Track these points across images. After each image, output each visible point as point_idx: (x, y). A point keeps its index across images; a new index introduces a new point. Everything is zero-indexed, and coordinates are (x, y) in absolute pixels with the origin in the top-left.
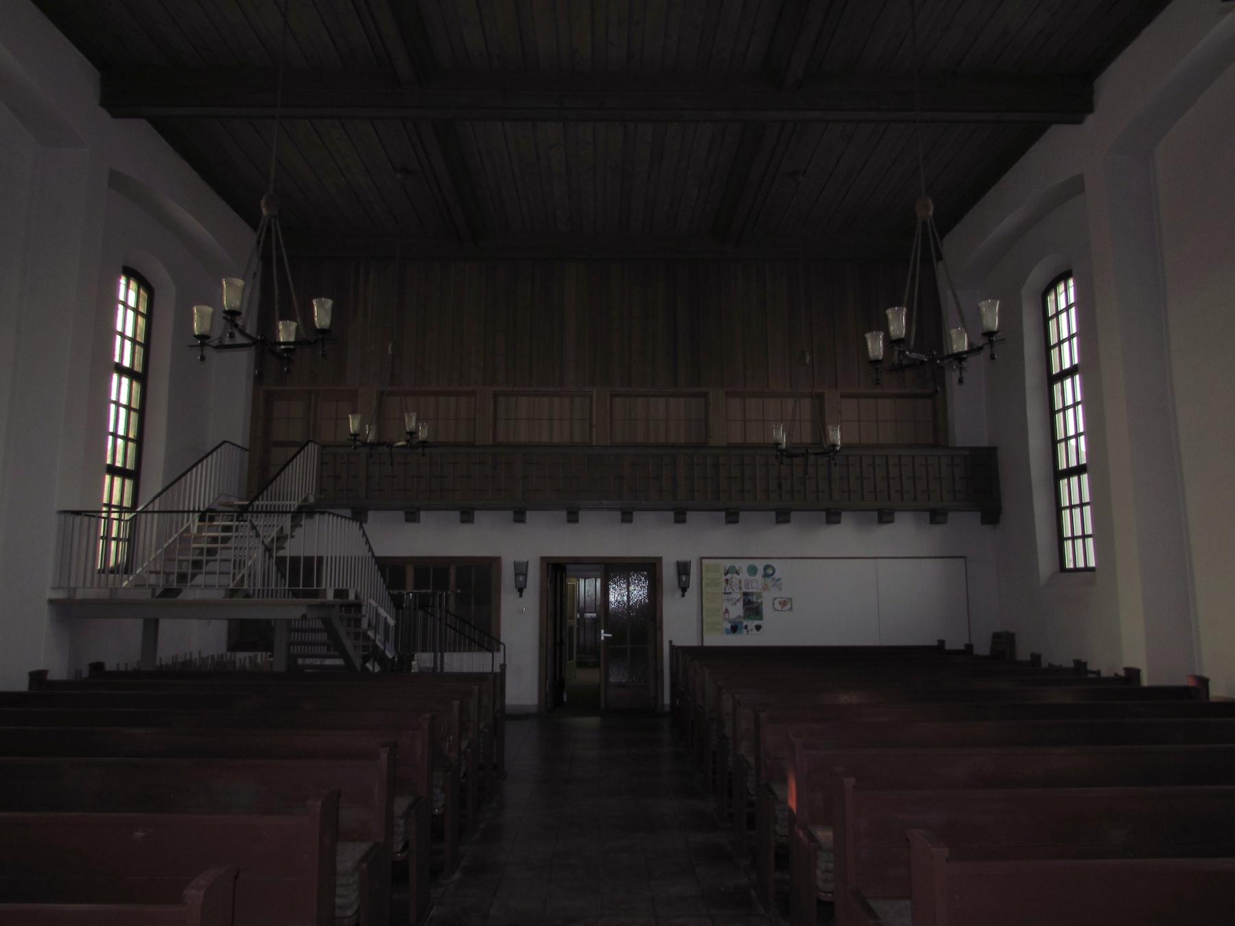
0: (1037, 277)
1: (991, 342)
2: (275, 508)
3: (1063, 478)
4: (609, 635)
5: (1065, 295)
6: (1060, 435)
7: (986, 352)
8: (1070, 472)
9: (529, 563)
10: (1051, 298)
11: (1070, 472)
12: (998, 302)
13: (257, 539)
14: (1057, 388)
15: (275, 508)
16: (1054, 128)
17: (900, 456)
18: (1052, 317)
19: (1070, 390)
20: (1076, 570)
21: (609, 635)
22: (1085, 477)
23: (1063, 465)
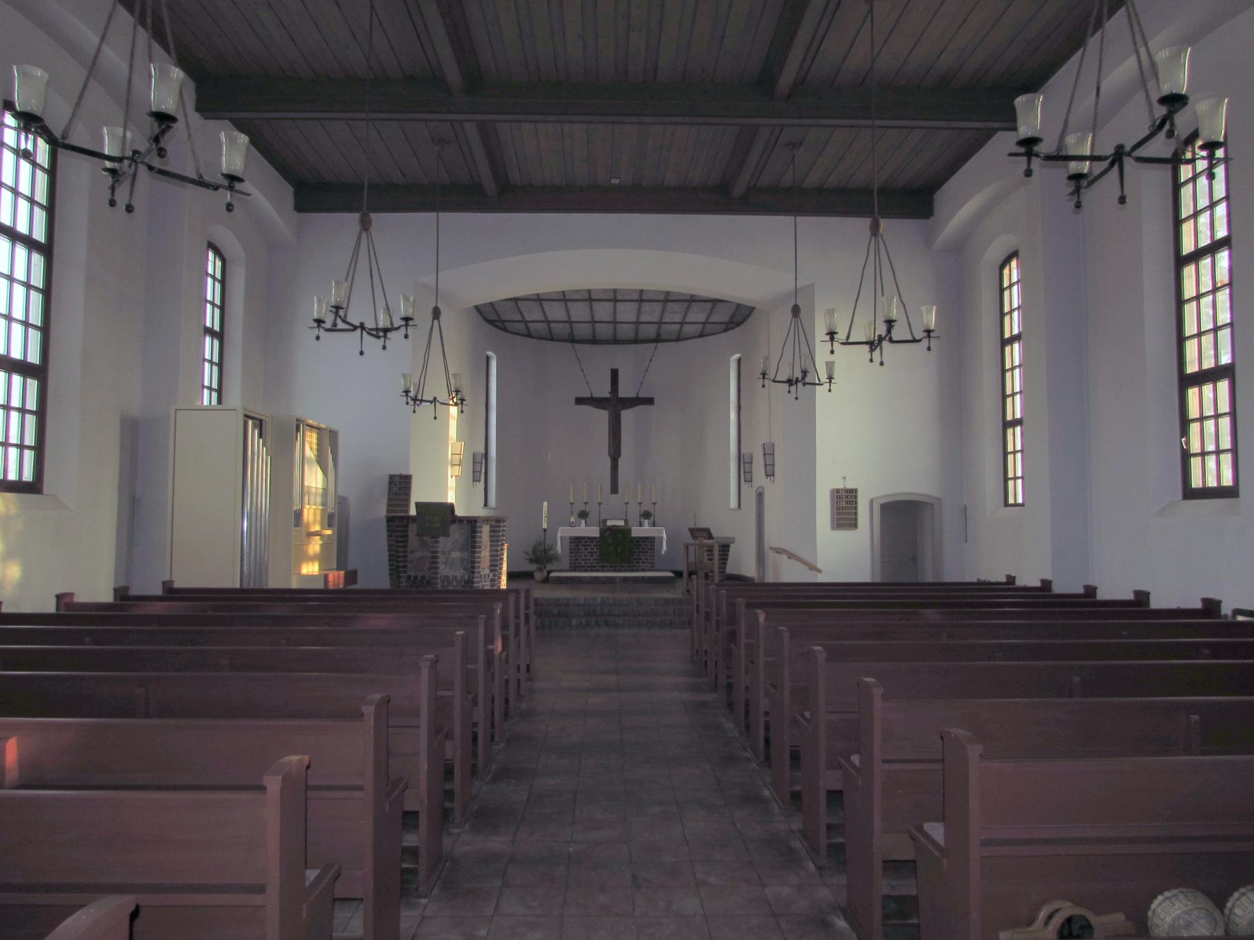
0: (994, 253)
1: (929, 337)
2: (572, 557)
3: (1192, 385)
4: (665, 548)
5: (1013, 272)
6: (1009, 392)
7: (925, 343)
8: (1202, 377)
9: (968, 508)
10: (1006, 271)
11: (1202, 377)
12: (935, 307)
13: (588, 510)
14: (1008, 349)
15: (572, 557)
16: (999, 133)
17: (745, 472)
18: (1187, 182)
19: (1015, 354)
20: (1016, 505)
21: (665, 548)
22: (1018, 429)
23: (1191, 368)
